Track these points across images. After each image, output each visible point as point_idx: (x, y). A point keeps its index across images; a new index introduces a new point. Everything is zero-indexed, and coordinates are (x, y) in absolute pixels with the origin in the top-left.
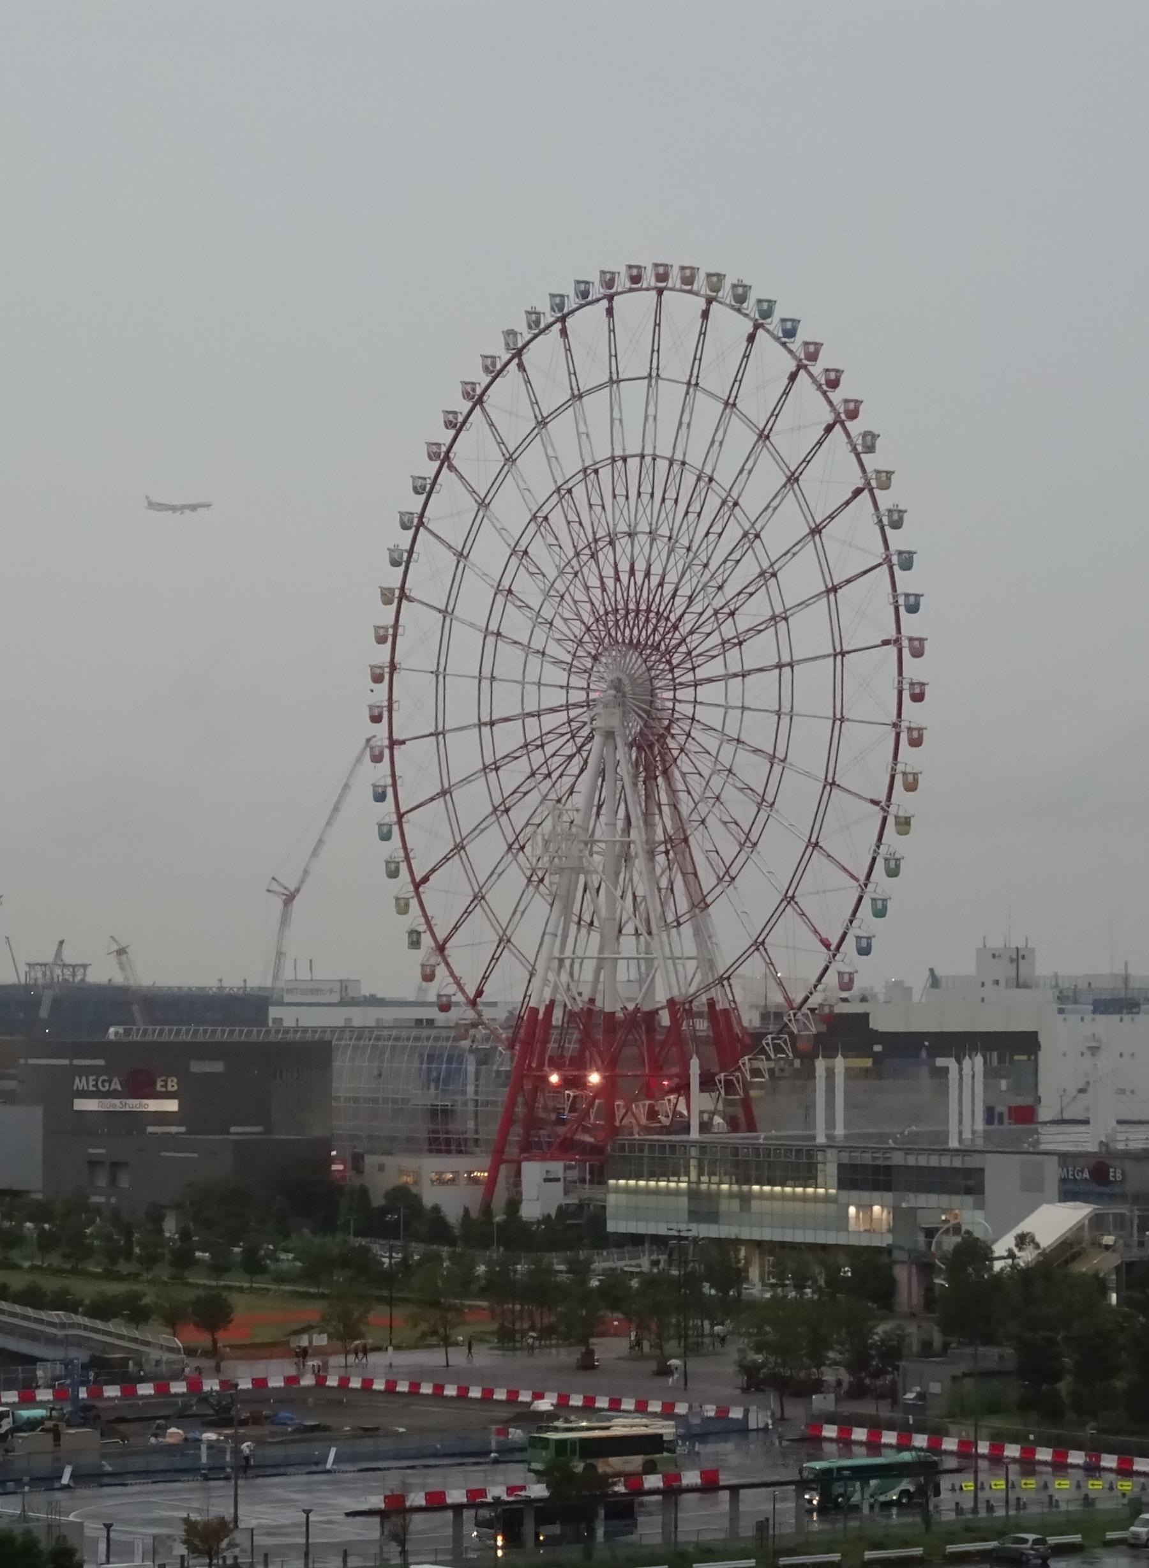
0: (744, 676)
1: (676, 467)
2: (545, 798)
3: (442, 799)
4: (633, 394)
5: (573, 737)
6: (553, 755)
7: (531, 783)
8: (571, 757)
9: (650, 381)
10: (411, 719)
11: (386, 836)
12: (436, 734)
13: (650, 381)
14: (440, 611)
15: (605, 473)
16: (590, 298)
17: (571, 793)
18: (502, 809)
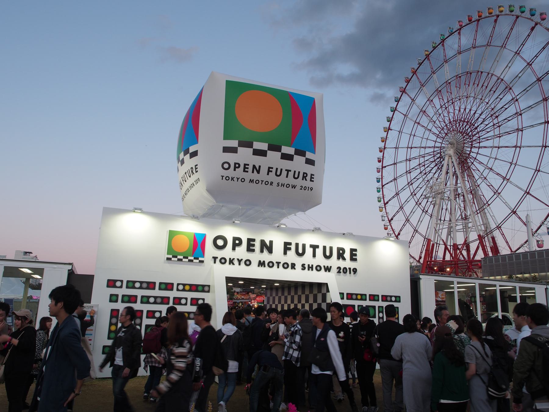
0: (499, 148)
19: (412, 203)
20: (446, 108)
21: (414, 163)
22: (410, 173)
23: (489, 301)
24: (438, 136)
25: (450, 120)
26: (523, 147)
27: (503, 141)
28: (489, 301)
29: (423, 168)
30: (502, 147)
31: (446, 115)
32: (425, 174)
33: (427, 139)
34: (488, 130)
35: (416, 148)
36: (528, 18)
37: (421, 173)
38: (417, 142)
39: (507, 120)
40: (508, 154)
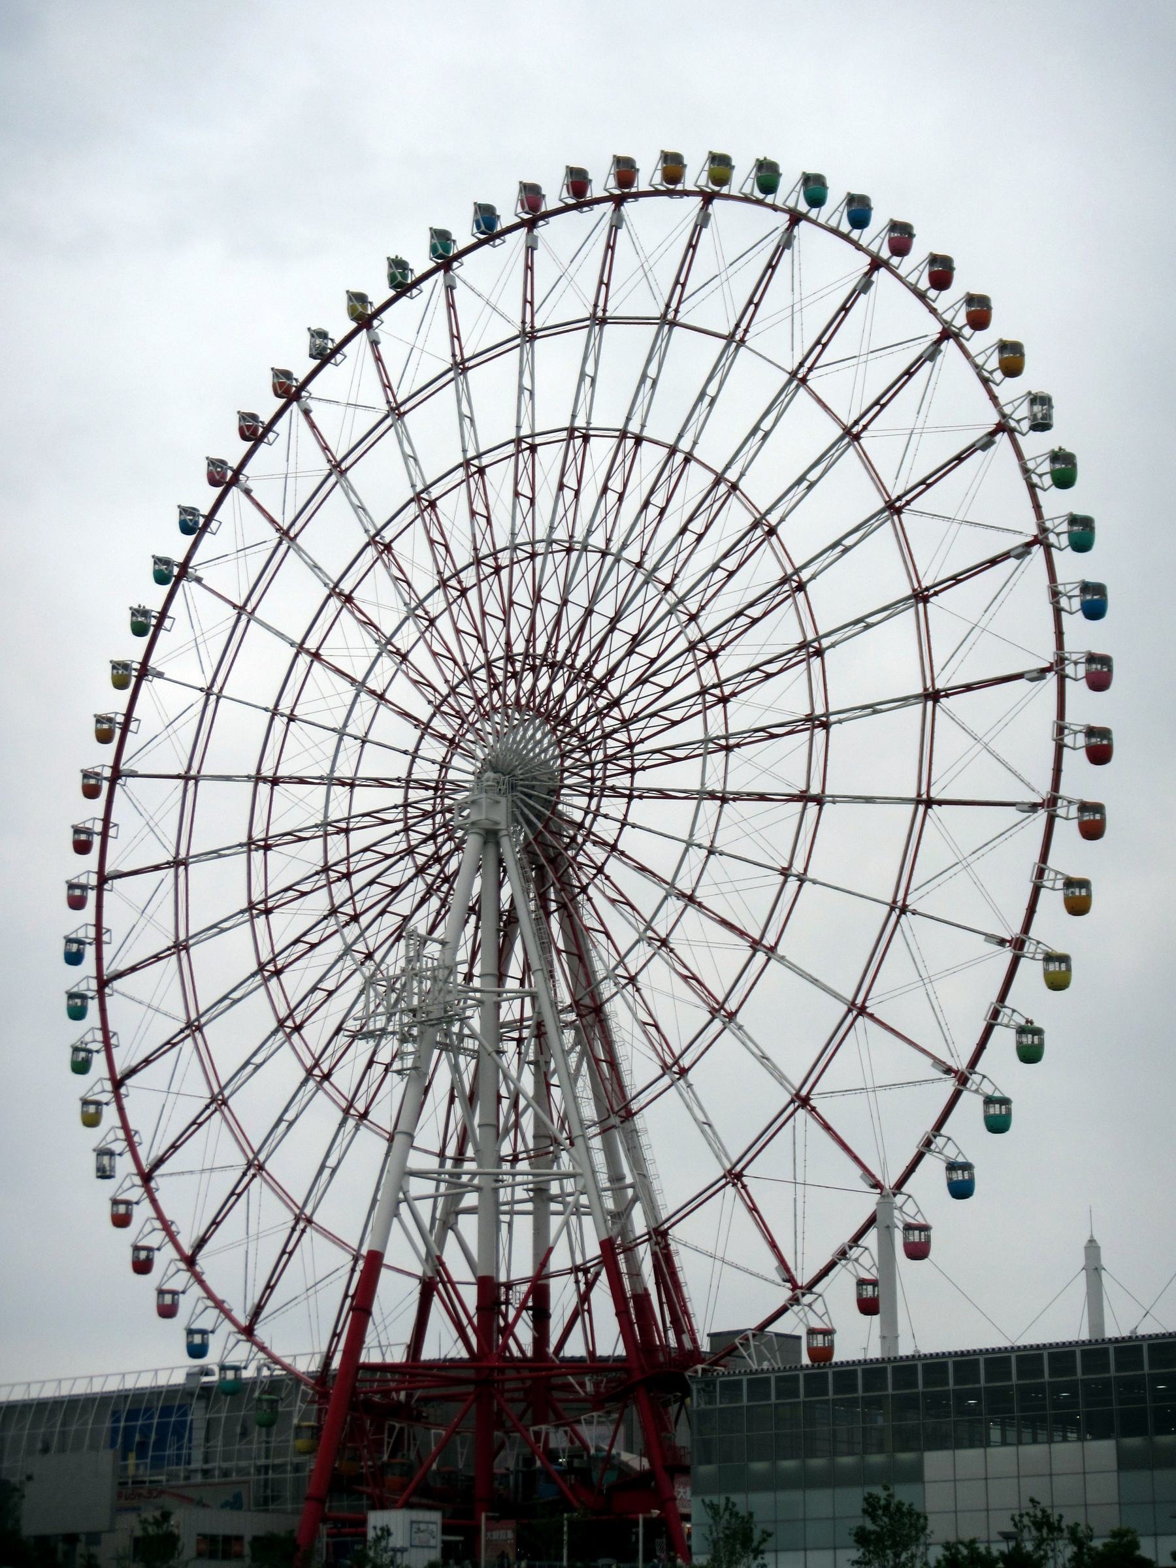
0: (724, 800)
1: (723, 488)
2: (348, 950)
3: (172, 870)
4: (624, 348)
5: (407, 829)
7: (332, 924)
9: (728, 346)
10: (157, 743)
11: (77, 903)
12: (186, 778)
13: (728, 346)
14: (235, 606)
18: (259, 909)
19: (284, 1070)
21: (290, 864)
22: (268, 912)
23: (727, 1528)
24: (425, 728)
25: (508, 644)
26: (835, 799)
27: (746, 770)
28: (727, 1528)
30: (739, 797)
32: (355, 918)
34: (675, 715)
35: (302, 781)
36: (835, 231)
37: (334, 911)
38: (306, 752)
39: (761, 673)
40: (768, 831)
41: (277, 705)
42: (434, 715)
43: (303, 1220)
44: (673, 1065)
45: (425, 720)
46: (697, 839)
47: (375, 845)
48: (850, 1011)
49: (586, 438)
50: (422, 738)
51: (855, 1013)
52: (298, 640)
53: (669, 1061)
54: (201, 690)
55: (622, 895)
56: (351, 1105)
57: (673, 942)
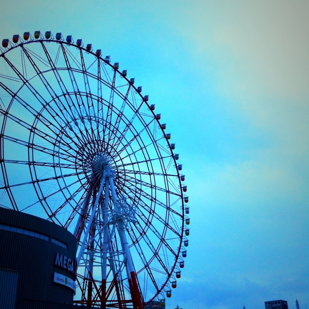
0: (67, 200)
5: (112, 146)
6: (115, 138)
8: (109, 140)
14: (163, 158)
15: (138, 235)
16: (29, 40)
17: (103, 130)
19: (94, 91)
20: (136, 192)
29: (112, 129)
31: (132, 187)
33: (129, 155)
37: (110, 124)
38: (135, 146)
41: (146, 148)
42: (124, 168)
43: (54, 69)
44: (32, 146)
45: (125, 166)
46: (66, 189)
47: (114, 140)
48: (8, 185)
49: (134, 243)
50: (123, 163)
51: (7, 186)
52: (151, 161)
53: (34, 147)
54: (157, 141)
55: (69, 168)
56: (69, 95)
57: (52, 168)
